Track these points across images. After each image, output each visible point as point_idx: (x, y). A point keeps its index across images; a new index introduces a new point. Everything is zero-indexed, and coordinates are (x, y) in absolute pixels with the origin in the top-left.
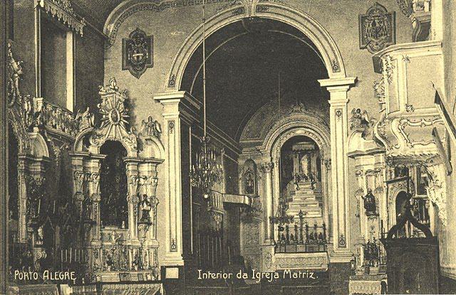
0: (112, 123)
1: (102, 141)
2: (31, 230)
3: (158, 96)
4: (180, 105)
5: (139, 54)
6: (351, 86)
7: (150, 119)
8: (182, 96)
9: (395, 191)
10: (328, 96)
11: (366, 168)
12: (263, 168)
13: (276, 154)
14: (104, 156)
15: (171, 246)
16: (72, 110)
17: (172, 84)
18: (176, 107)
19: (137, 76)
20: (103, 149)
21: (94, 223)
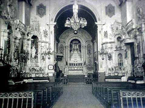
0: (35, 30)
1: (32, 35)
2: (15, 60)
3: (45, 25)
4: (54, 27)
5: (41, 10)
6: (104, 25)
7: (46, 30)
8: (55, 24)
9: (118, 53)
10: (97, 27)
11: (108, 47)
12: (65, 47)
13: (69, 43)
14: (33, 40)
15: (66, 64)
16: (24, 23)
17: (52, 20)
18: (53, 27)
19: (41, 17)
20: (32, 38)
21: (29, 59)
